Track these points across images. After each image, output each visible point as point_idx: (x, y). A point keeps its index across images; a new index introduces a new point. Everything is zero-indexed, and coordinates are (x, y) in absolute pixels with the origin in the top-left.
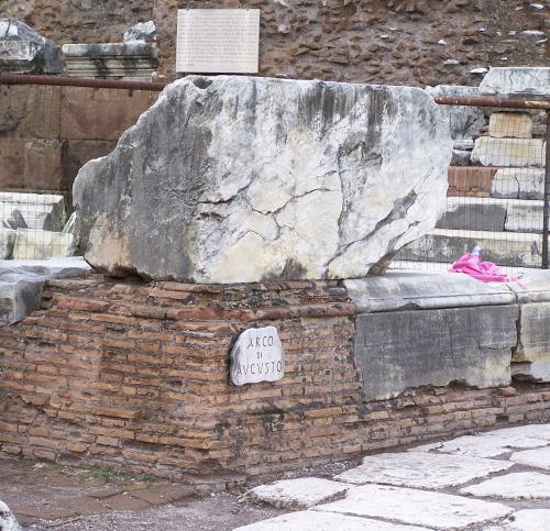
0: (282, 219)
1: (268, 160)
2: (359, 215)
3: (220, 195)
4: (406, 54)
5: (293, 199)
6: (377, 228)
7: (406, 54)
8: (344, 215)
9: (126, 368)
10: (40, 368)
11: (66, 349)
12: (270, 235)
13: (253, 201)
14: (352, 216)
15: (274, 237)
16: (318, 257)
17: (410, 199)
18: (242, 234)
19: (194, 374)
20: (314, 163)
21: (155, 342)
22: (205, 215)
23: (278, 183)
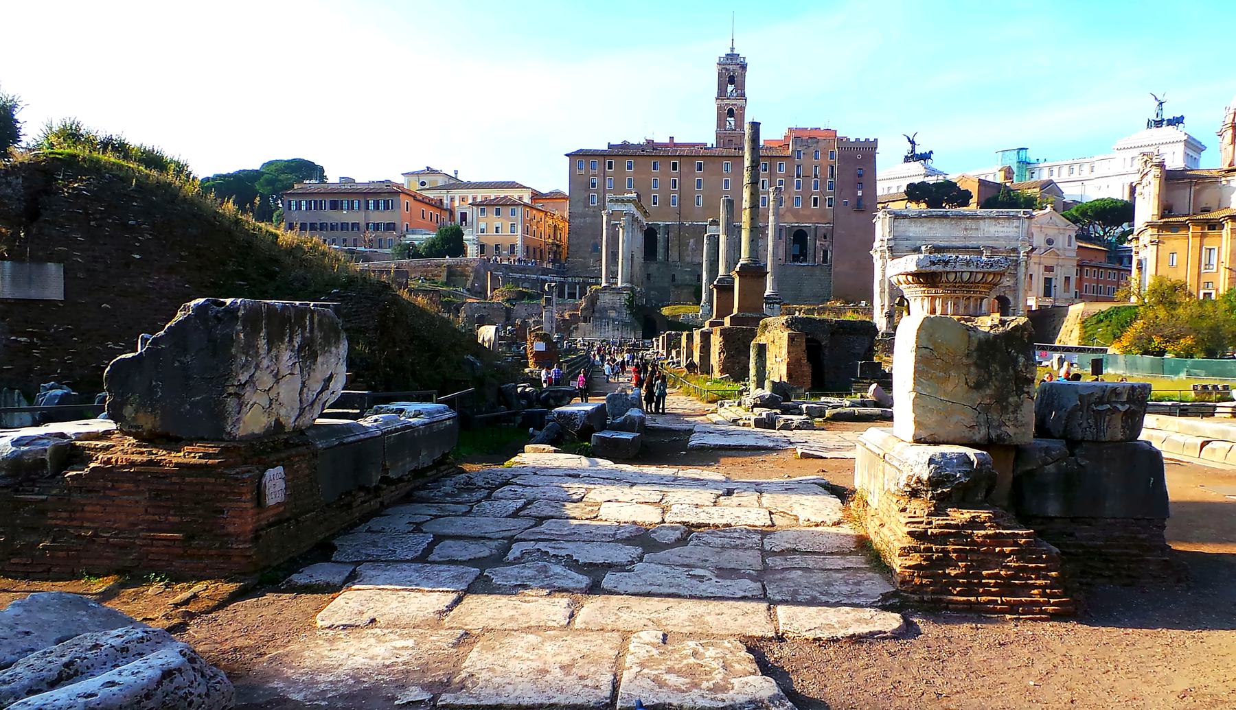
0: (273, 395)
1: (264, 356)
2: (309, 389)
3: (240, 380)
4: (165, 291)
5: (277, 382)
6: (317, 396)
7: (165, 291)
8: (302, 390)
9: (169, 504)
10: (86, 508)
11: (112, 493)
12: (266, 405)
13: (257, 384)
14: (305, 390)
15: (268, 406)
16: (290, 417)
17: (331, 376)
18: (252, 405)
19: (235, 505)
20: (286, 358)
21: (197, 484)
22: (230, 394)
23: (269, 370)
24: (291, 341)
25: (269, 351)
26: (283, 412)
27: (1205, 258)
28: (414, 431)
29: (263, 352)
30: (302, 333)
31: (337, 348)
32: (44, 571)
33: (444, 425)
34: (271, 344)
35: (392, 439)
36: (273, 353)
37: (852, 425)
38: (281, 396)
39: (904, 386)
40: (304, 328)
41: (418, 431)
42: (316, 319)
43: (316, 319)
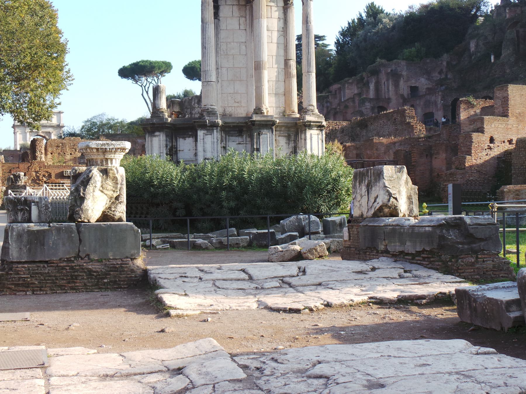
17: (377, 196)
24: (365, 182)
25: (359, 187)
26: (363, 210)
27: (309, 53)
28: (401, 229)
29: (358, 187)
30: (368, 179)
31: (379, 183)
32: (486, 261)
33: (423, 230)
34: (360, 184)
35: (388, 229)
36: (360, 187)
37: (266, 267)
38: (363, 203)
39: (498, 375)
40: (368, 177)
41: (404, 229)
42: (372, 171)
43: (372, 171)
